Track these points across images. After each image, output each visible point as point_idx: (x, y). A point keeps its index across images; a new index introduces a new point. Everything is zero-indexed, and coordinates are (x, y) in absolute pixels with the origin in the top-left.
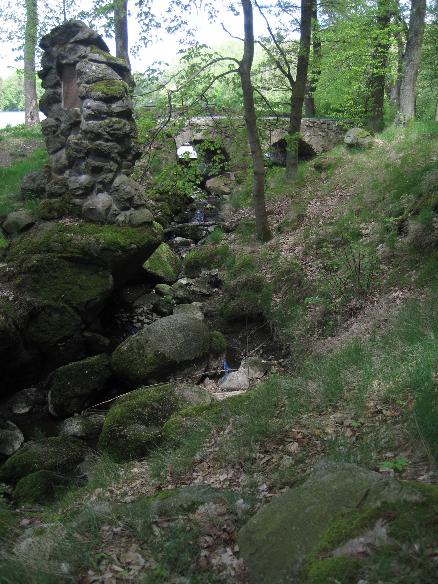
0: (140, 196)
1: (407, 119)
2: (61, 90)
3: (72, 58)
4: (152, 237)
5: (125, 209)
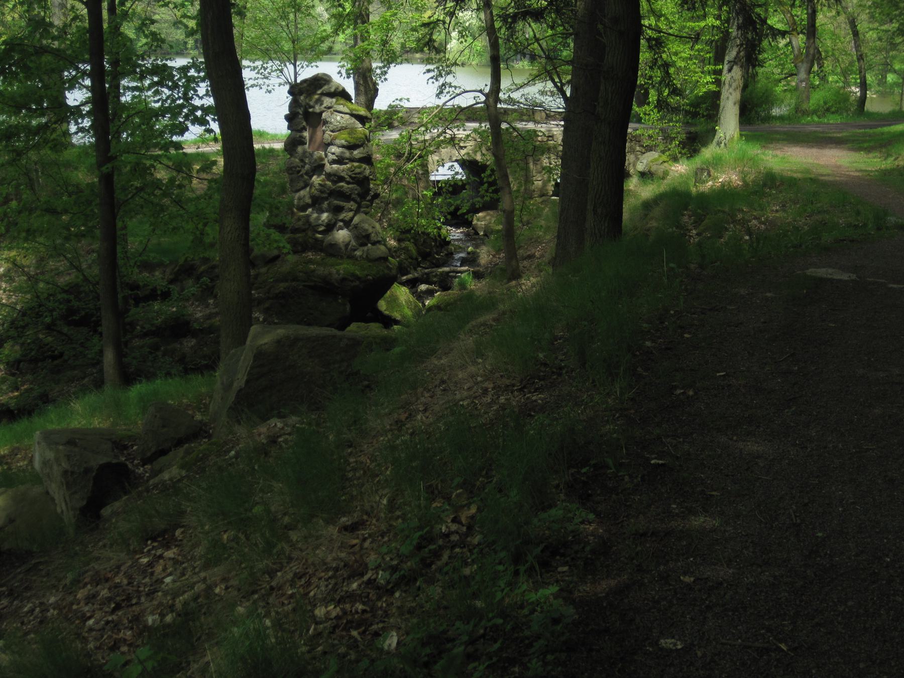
0: (377, 233)
1: (727, 138)
2: (306, 134)
3: (317, 109)
4: (386, 271)
5: (363, 244)
